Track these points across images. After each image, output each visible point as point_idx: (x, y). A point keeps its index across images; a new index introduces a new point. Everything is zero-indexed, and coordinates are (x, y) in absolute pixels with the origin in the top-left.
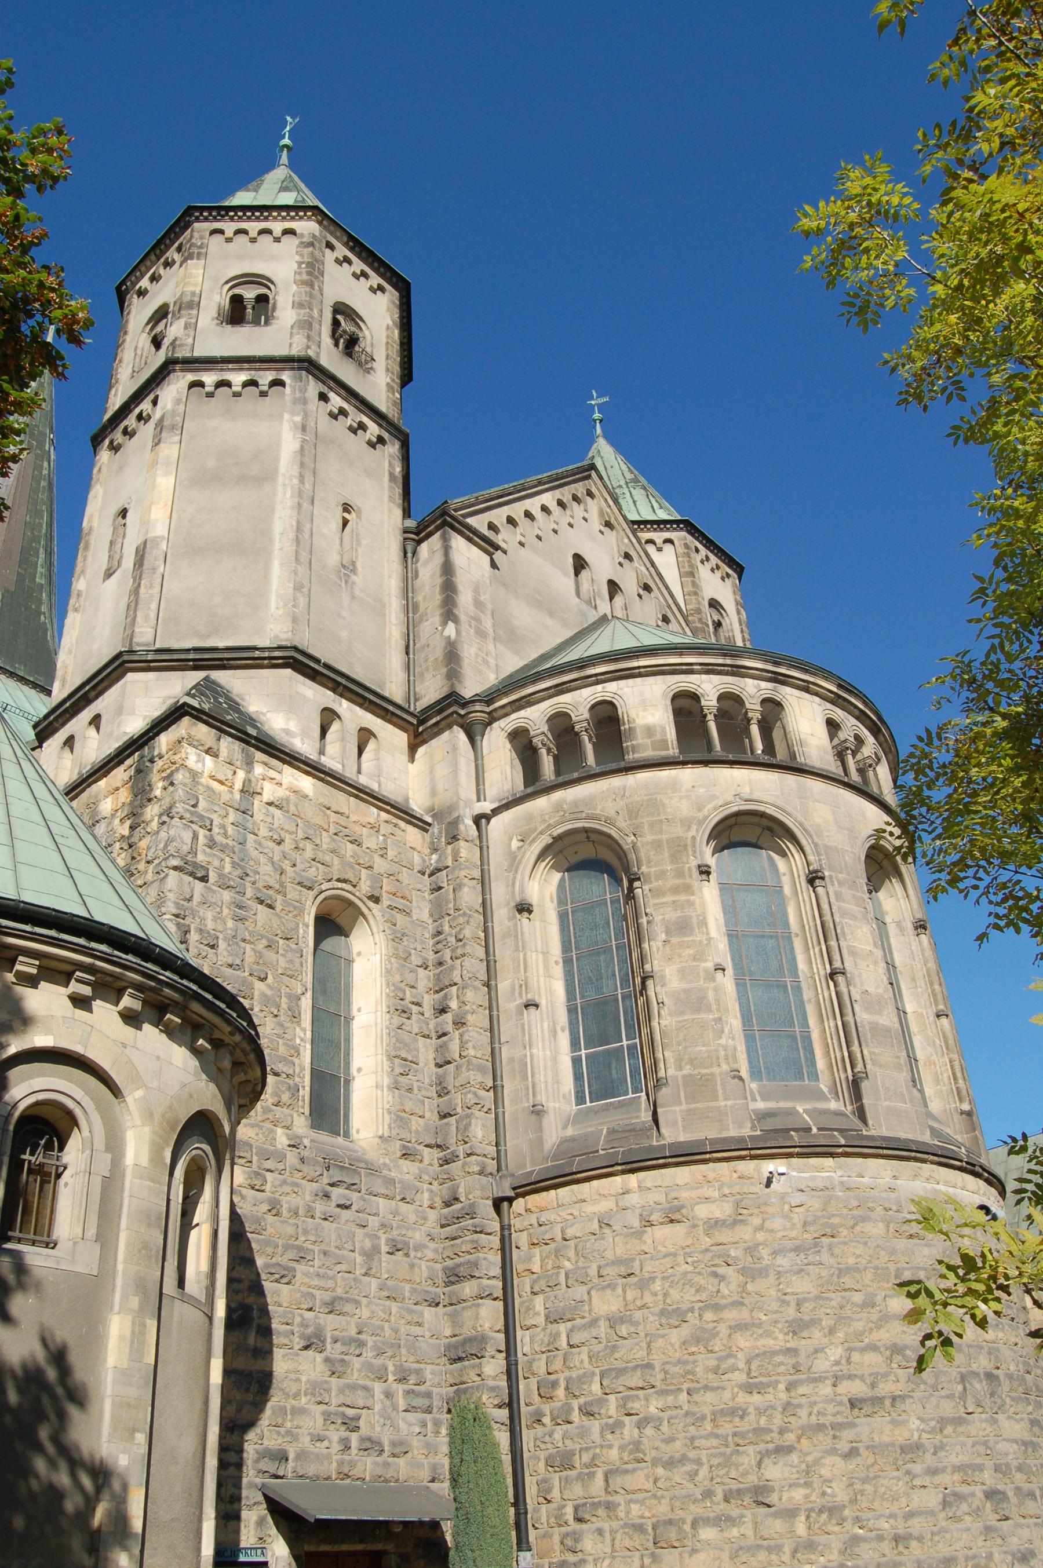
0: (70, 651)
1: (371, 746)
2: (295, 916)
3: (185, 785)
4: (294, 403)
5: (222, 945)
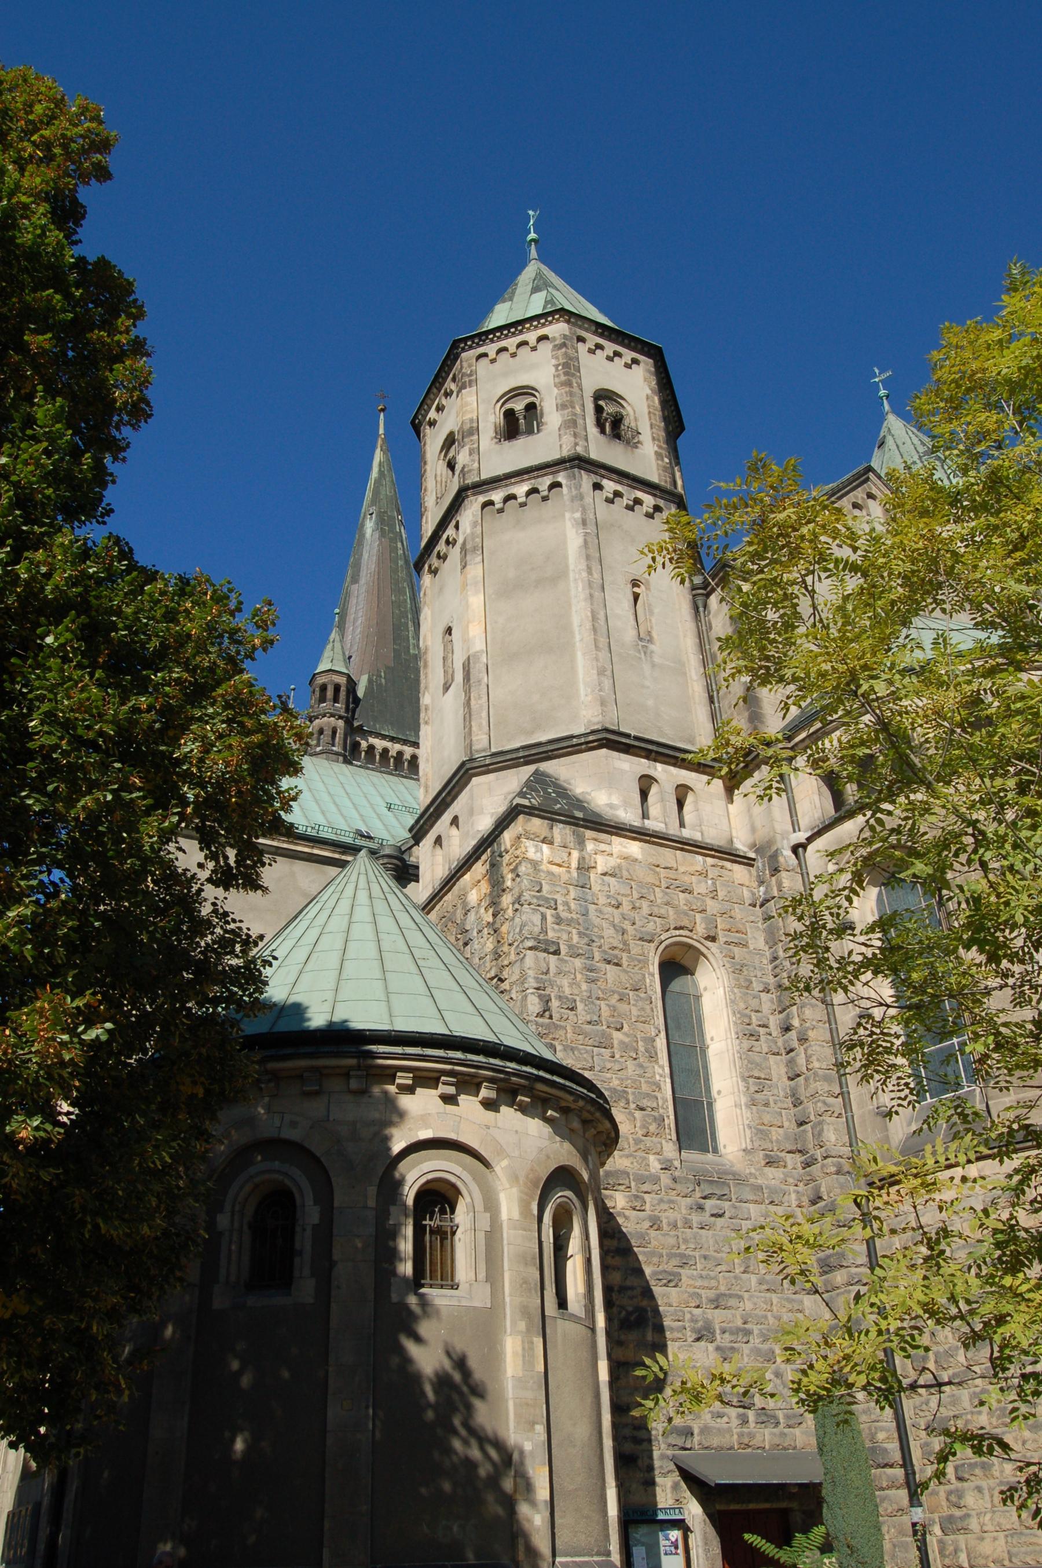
0: (427, 760)
1: (690, 799)
2: (641, 969)
3: (528, 875)
4: (572, 501)
5: (580, 1006)
